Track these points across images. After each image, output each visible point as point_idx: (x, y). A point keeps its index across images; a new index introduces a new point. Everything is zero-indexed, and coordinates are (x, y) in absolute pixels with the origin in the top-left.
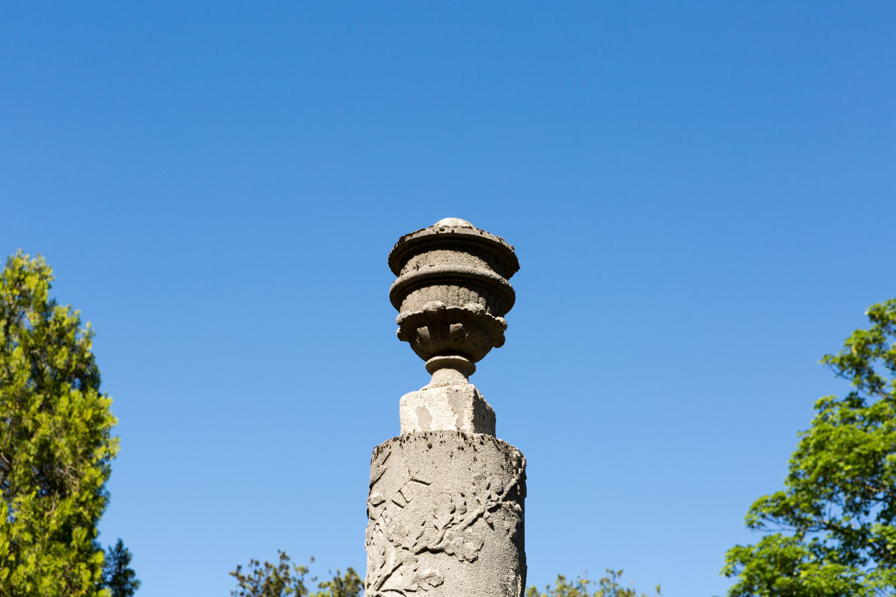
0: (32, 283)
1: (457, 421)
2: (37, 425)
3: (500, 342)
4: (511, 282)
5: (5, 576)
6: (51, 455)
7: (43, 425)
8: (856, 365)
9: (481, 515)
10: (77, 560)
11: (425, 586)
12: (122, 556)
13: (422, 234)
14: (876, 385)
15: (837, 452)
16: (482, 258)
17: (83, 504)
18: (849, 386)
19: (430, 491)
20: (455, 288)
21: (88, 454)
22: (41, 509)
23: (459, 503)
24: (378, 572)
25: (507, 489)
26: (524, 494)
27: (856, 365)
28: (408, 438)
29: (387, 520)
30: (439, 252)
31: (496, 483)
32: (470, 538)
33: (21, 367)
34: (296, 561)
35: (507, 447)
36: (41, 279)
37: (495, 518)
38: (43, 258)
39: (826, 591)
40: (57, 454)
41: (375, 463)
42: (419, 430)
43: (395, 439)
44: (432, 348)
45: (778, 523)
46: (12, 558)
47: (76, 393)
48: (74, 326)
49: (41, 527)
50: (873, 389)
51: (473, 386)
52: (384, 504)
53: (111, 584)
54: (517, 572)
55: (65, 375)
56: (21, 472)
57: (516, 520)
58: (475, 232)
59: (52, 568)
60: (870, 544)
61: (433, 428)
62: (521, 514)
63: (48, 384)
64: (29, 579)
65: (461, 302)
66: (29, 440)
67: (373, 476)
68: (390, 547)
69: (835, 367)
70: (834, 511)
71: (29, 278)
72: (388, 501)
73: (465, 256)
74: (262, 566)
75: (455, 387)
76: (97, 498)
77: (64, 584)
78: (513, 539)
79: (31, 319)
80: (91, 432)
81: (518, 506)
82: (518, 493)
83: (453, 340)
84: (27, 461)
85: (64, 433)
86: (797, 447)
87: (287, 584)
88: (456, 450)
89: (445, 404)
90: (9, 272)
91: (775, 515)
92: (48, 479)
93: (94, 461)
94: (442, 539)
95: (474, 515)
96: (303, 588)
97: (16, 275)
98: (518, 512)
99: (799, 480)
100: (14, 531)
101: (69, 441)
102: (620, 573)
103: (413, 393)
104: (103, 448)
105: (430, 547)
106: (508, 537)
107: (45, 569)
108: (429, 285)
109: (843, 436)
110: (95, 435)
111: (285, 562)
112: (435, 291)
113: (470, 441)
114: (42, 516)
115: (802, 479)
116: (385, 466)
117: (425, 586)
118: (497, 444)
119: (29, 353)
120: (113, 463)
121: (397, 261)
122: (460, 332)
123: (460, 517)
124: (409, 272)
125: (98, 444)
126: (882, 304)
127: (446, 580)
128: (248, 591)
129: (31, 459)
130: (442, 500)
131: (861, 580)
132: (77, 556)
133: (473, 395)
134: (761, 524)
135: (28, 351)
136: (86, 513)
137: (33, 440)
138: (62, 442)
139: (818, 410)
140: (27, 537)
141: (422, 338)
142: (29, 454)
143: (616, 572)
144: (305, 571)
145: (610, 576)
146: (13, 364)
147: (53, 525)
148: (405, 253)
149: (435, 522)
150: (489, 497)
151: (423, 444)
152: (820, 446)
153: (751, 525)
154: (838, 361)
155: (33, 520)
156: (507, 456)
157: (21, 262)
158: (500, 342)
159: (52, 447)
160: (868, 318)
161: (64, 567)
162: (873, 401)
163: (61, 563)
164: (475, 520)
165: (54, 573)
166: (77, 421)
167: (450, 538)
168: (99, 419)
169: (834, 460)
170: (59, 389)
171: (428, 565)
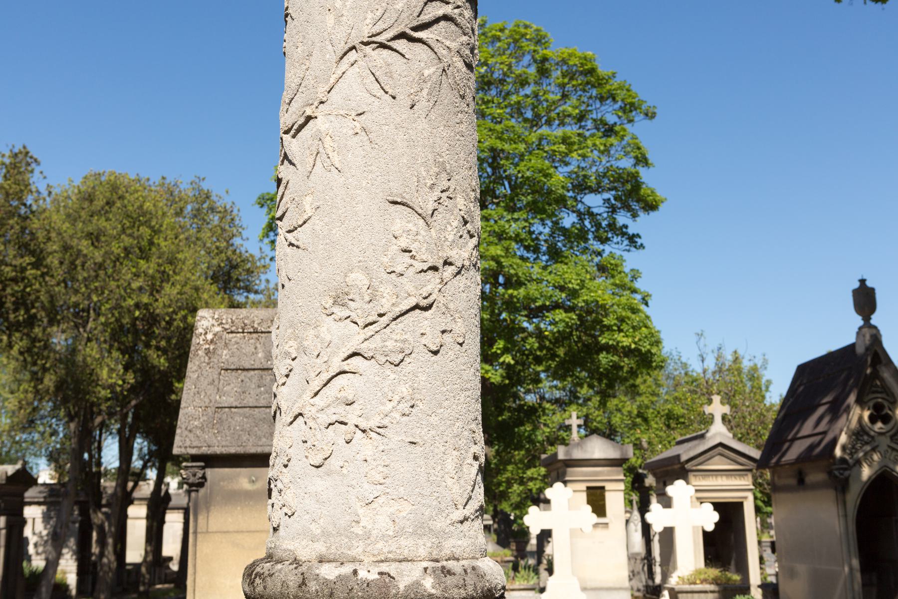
102: (203, 179)
145: (197, 181)
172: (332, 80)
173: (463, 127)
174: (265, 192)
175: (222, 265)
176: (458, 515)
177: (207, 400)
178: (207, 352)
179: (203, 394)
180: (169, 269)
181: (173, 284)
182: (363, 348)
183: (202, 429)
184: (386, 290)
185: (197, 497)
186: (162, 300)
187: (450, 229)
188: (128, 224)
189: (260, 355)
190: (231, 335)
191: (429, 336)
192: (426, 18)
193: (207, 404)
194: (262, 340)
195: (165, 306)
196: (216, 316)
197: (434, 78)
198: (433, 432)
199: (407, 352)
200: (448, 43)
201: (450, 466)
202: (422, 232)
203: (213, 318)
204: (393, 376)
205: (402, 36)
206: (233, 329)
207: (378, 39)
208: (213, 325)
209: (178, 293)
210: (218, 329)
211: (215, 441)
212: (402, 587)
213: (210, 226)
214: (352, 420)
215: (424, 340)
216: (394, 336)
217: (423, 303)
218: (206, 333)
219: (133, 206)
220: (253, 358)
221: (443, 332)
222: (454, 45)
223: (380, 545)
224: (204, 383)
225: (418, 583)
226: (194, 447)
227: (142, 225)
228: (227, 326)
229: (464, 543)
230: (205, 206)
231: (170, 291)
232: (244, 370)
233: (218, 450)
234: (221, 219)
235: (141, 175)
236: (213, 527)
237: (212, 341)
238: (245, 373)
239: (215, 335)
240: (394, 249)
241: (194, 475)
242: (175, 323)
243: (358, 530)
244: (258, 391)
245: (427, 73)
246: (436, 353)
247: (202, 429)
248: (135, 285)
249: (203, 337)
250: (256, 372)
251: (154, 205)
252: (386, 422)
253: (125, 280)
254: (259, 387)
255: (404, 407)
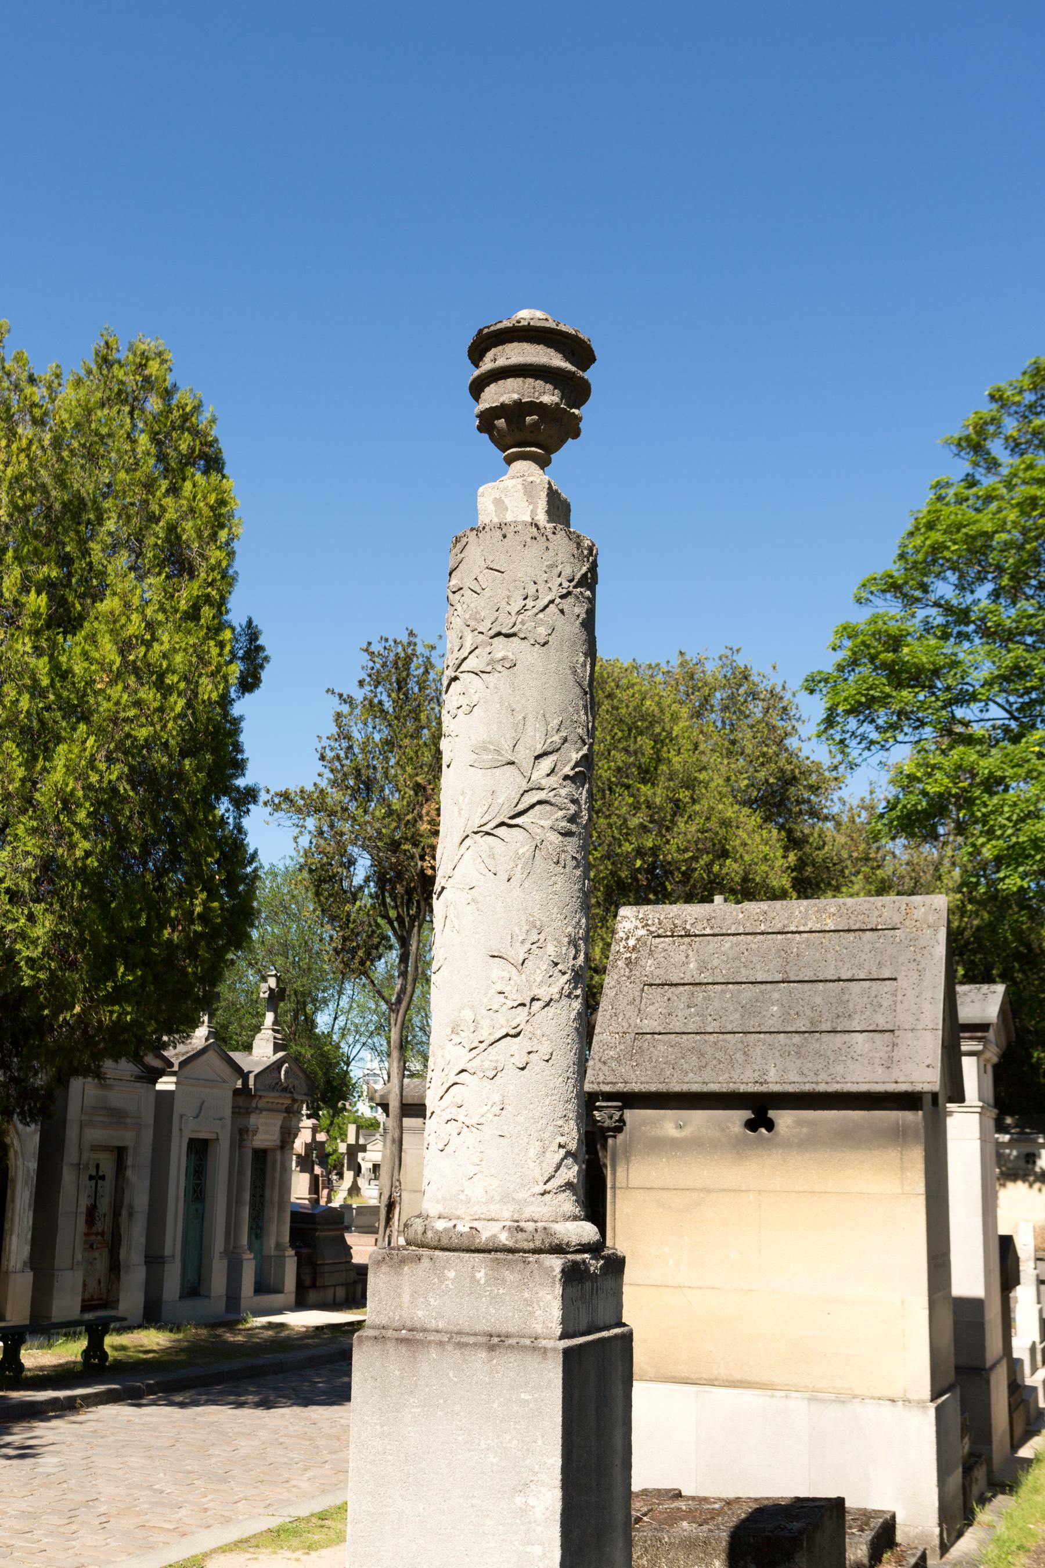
0: (153, 368)
1: (532, 511)
2: (163, 509)
3: (576, 434)
4: (586, 375)
5: (142, 654)
6: (179, 537)
7: (169, 510)
8: (975, 445)
9: (552, 602)
10: (207, 638)
11: (499, 668)
12: (252, 633)
13: (499, 326)
14: (993, 465)
15: (945, 532)
16: (558, 350)
17: (211, 584)
18: (966, 467)
19: (504, 579)
20: (530, 380)
21: (214, 536)
22: (171, 590)
23: (531, 590)
24: (456, 654)
25: (578, 577)
26: (595, 581)
27: (975, 445)
28: (484, 528)
29: (465, 606)
30: (515, 344)
31: (567, 571)
32: (541, 623)
33: (148, 453)
34: (423, 640)
35: (579, 536)
36: (161, 364)
37: (566, 604)
38: (161, 341)
39: (927, 666)
40: (184, 537)
41: (454, 551)
42: (496, 520)
43: (472, 529)
44: (509, 440)
45: (885, 600)
46: (148, 637)
47: (199, 477)
48: (197, 408)
49: (172, 607)
50: (989, 469)
51: (547, 478)
52: (461, 592)
53: (242, 659)
54: (586, 655)
55: (188, 460)
56: (150, 555)
57: (586, 606)
58: (551, 324)
59: (183, 645)
60: (973, 622)
61: (509, 518)
62: (592, 601)
63: (174, 470)
64: (165, 656)
65: (537, 394)
66: (157, 524)
67: (452, 564)
68: (467, 632)
69: (953, 448)
70: (944, 589)
71: (151, 363)
72: (465, 588)
73: (540, 349)
74: (391, 642)
75: (530, 479)
76: (226, 578)
77: (194, 660)
78: (583, 624)
79: (154, 404)
80: (215, 515)
81: (588, 593)
82: (589, 581)
83: (528, 434)
84: (156, 544)
85: (189, 517)
86: (910, 526)
87: (415, 659)
88: (529, 540)
89: (520, 494)
90: (131, 357)
91: (884, 591)
92: (177, 561)
93: (218, 543)
94: (515, 624)
95: (546, 601)
96: (431, 664)
97: (138, 360)
98: (588, 598)
99: (906, 560)
100: (149, 612)
101: (195, 525)
102: (738, 651)
103: (490, 484)
104: (226, 530)
105: (504, 631)
106: (578, 622)
107: (177, 646)
108: (505, 378)
109: (952, 517)
110: (219, 518)
111: (412, 639)
112: (512, 383)
113: (543, 531)
114: (173, 596)
115: (911, 559)
116: (462, 555)
117: (499, 668)
118: (569, 534)
119: (154, 439)
120: (236, 545)
121: (477, 353)
122: (535, 424)
123: (532, 604)
124: (487, 364)
125: (222, 526)
126: (1003, 385)
127: (518, 663)
128: (378, 666)
129: (159, 542)
130: (516, 587)
131: (961, 656)
132: (206, 634)
133: (547, 486)
134: (867, 599)
135: (155, 439)
136: (214, 593)
137: (161, 524)
138: (188, 525)
139: (933, 491)
140: (161, 617)
141: (499, 431)
142: (158, 538)
143: (735, 649)
144: (433, 648)
145: (729, 653)
146: (139, 450)
147: (183, 605)
148: (483, 346)
149: (508, 608)
150: (561, 585)
151: (498, 534)
152: (931, 526)
153: (859, 601)
154: (956, 442)
155: (164, 600)
156: (579, 545)
157: (143, 347)
158: (576, 434)
159: (179, 529)
160: (988, 398)
161: (194, 645)
162: (988, 482)
163: (192, 640)
164: (547, 606)
165: (185, 650)
166: (202, 504)
167: (523, 623)
168: (222, 503)
169: (941, 540)
170: (183, 473)
171: (502, 648)
172: (456, 861)
173: (557, 887)
174: (815, 670)
175: (771, 780)
176: (541, 1188)
177: (626, 1025)
178: (629, 962)
179: (621, 1016)
180: (684, 795)
181: (690, 817)
182: (468, 1066)
183: (618, 1060)
184: (485, 1024)
185: (615, 1144)
186: (676, 841)
187: (538, 971)
188: (620, 734)
189: (691, 966)
190: (658, 940)
191: (517, 1057)
192: (521, 807)
193: (625, 1030)
194: (695, 946)
195: (679, 850)
196: (641, 916)
197: (527, 855)
198: (519, 1128)
199: (499, 1069)
200: (542, 823)
201: (532, 1152)
202: (515, 978)
203: (637, 918)
204: (489, 1087)
205: (502, 824)
206: (661, 931)
207: (485, 829)
208: (637, 928)
209: (699, 831)
210: (642, 932)
211: (633, 1076)
212: (484, 1239)
213: (750, 721)
214: (461, 1118)
215: (513, 1060)
216: (490, 1058)
217: (513, 1032)
218: (627, 938)
219: (627, 706)
220: (683, 969)
221: (529, 1053)
222: (547, 823)
223: (475, 1209)
224: (623, 1003)
225: (495, 1236)
226: (608, 1083)
227: (641, 734)
228: (653, 929)
229: (545, 1209)
230: (742, 691)
231: (686, 830)
232: (672, 985)
233: (636, 1087)
234: (767, 711)
235: (639, 662)
236: (634, 1182)
237: (634, 948)
238: (673, 989)
239: (638, 940)
240: (493, 992)
241: (611, 1117)
242: (696, 875)
243: (462, 1197)
244: (687, 1012)
245: (521, 851)
246: (523, 1069)
247: (618, 1060)
248: (634, 822)
249: (624, 942)
250: (686, 987)
251: (658, 704)
252: (481, 1121)
253: (619, 816)
254: (689, 1007)
255: (496, 1110)
